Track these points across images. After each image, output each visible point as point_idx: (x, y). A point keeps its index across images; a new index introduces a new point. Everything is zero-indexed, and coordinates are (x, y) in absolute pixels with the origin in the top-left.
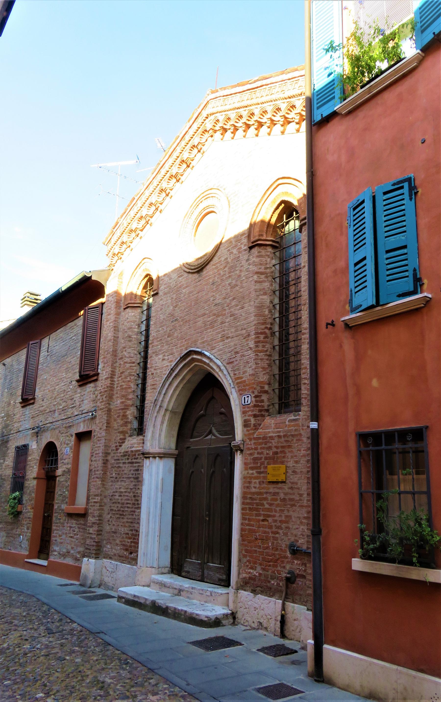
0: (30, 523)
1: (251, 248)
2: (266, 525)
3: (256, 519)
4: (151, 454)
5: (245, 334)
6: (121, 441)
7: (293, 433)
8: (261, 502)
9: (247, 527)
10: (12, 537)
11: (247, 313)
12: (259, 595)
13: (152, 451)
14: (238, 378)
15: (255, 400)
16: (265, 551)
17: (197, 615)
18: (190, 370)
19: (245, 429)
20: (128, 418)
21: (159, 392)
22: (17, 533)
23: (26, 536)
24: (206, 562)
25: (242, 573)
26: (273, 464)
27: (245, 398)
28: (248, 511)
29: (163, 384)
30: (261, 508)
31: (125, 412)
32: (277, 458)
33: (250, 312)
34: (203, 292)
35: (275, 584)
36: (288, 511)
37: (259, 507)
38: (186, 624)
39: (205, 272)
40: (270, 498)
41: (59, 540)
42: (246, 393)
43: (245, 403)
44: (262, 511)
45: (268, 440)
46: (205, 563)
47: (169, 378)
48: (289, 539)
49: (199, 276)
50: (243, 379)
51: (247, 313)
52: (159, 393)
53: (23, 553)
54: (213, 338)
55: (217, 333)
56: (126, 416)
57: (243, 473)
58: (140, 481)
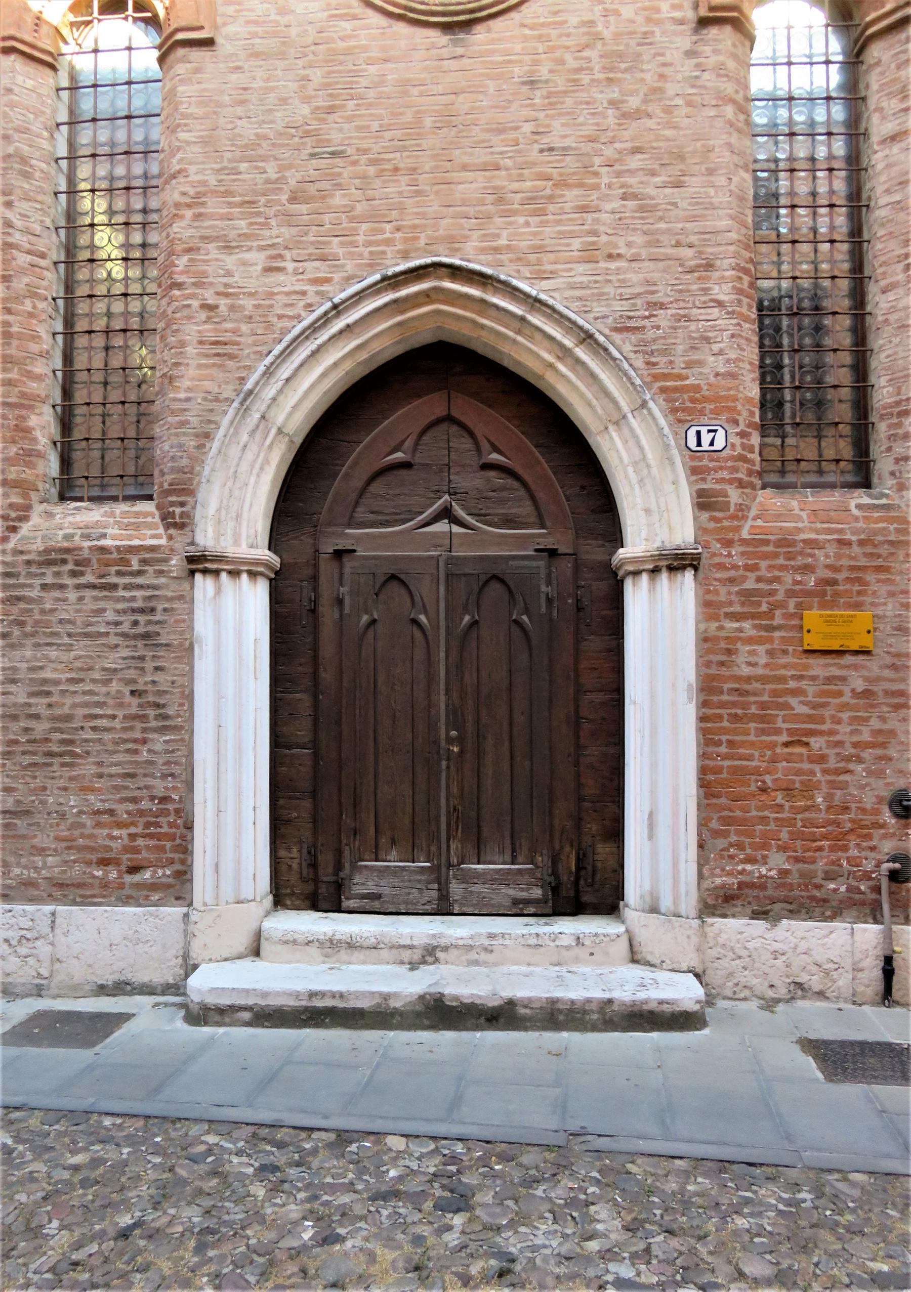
1: (704, 23)
2: (802, 755)
3: (762, 742)
4: (228, 563)
5: (691, 259)
6: (13, 515)
7: (892, 538)
8: (780, 700)
9: (727, 763)
11: (697, 203)
12: (785, 922)
13: (231, 550)
14: (665, 377)
16: (799, 816)
17: (661, 1002)
18: (399, 324)
19: (705, 516)
20: (35, 440)
21: (268, 368)
24: (455, 860)
25: (713, 875)
26: (819, 609)
27: (698, 433)
28: (726, 724)
29: (288, 346)
30: (777, 715)
31: (24, 418)
32: (836, 594)
33: (711, 203)
34: (481, 97)
35: (843, 889)
36: (883, 719)
37: (769, 712)
38: (616, 1034)
39: (480, 35)
40: (811, 690)
42: (705, 420)
43: (699, 444)
44: (784, 722)
45: (798, 549)
46: (449, 865)
47: (314, 331)
48: (888, 784)
49: (455, 43)
50: (687, 382)
51: (697, 203)
52: (265, 373)
54: (541, 246)
55: (560, 232)
56: (28, 431)
57: (703, 626)
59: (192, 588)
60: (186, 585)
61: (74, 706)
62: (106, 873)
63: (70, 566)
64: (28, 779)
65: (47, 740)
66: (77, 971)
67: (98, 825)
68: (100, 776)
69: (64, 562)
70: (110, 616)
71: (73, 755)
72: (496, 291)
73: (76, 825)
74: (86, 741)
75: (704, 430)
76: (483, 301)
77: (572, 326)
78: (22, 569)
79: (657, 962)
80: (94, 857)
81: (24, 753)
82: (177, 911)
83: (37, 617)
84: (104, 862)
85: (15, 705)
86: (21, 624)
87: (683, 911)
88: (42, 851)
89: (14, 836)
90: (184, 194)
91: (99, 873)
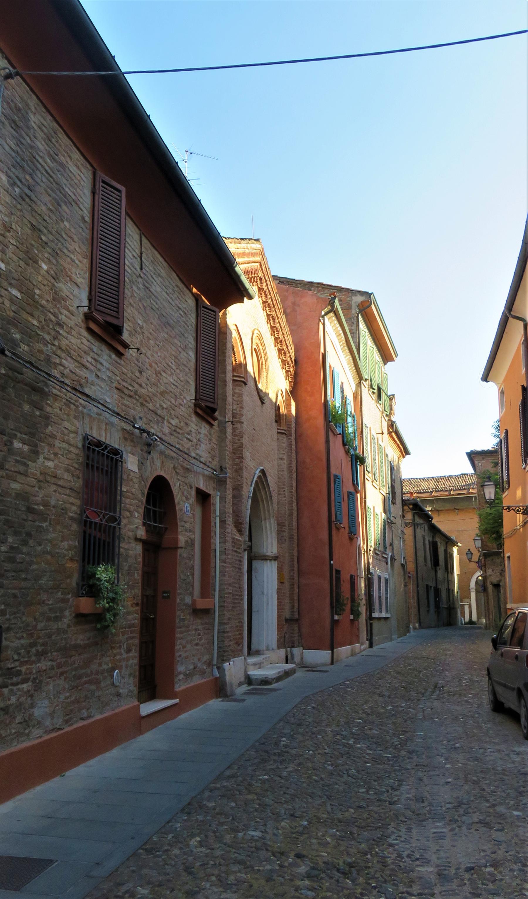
0: (133, 638)
10: (90, 682)
15: (37, 447)
22: (105, 667)
23: (127, 667)
41: (183, 655)
53: (123, 708)
58: (407, 630)
82: (243, 657)
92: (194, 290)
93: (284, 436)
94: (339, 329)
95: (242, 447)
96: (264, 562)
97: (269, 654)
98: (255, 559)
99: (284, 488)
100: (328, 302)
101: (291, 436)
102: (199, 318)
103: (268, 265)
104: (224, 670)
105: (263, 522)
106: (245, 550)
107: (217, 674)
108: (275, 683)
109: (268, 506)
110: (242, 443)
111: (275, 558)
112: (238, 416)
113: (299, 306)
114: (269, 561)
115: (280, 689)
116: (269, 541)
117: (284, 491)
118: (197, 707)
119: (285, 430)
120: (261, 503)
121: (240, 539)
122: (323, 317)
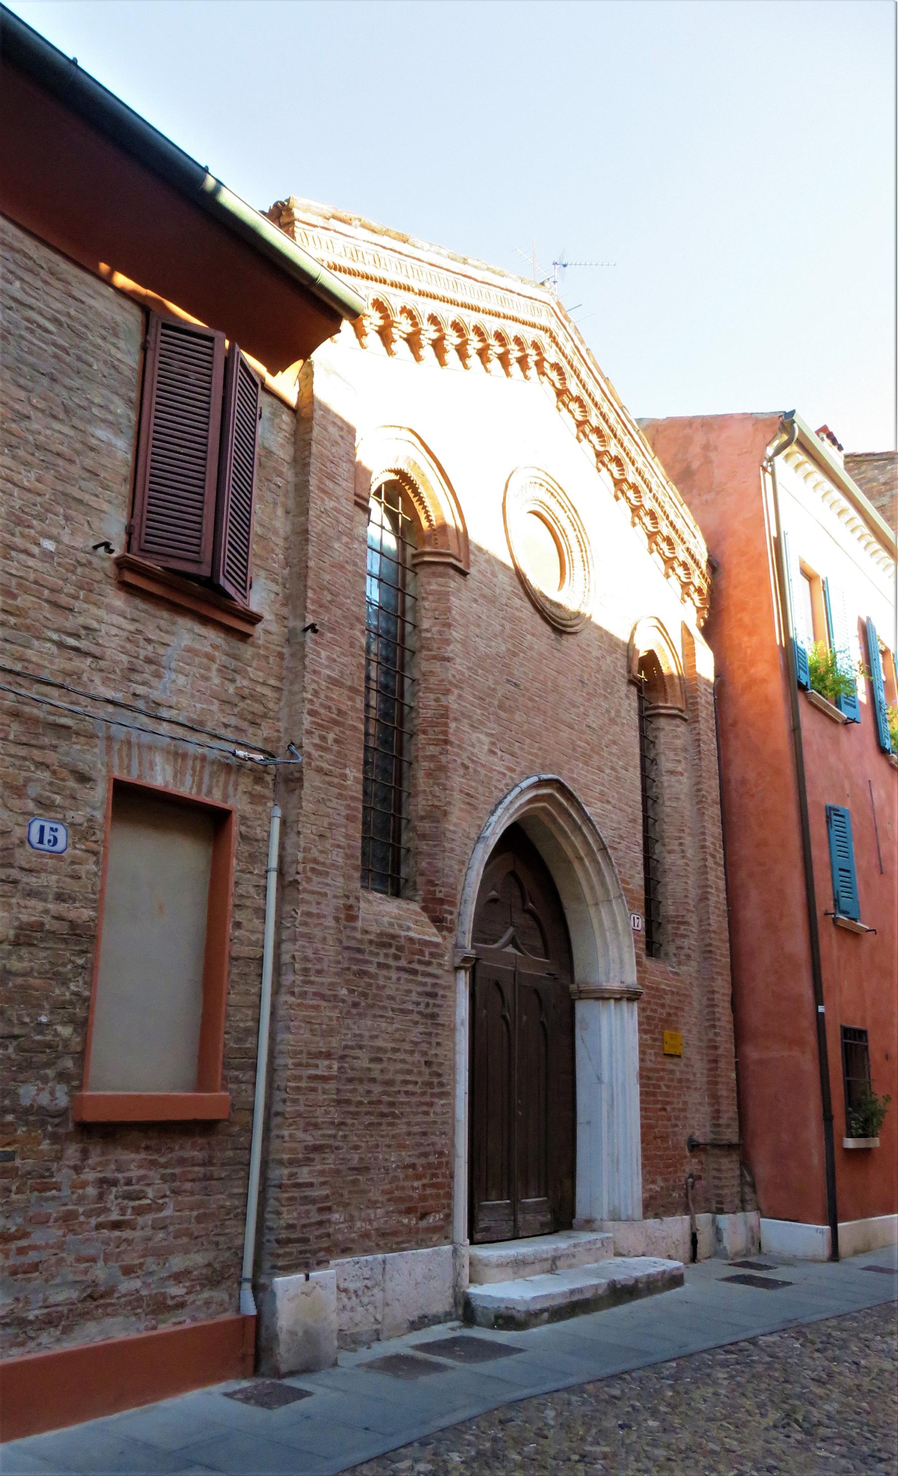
27: (42, 828)
59: (456, 980)
60: (452, 978)
61: (397, 1072)
62: (410, 1220)
63: (393, 951)
64: (368, 1138)
65: (380, 1102)
66: (401, 1314)
67: (406, 1178)
68: (409, 1134)
69: (390, 945)
70: (414, 997)
71: (393, 1114)
72: (572, 805)
73: (395, 1179)
74: (402, 1103)
75: (48, 826)
76: (567, 810)
77: (599, 840)
78: (366, 947)
79: (625, 1252)
80: (402, 1207)
81: (367, 1113)
82: (448, 1248)
83: (375, 991)
84: (409, 1211)
85: (362, 1068)
86: (365, 995)
87: (636, 1217)
88: (373, 1204)
89: (357, 1192)
90: (454, 676)
91: (406, 1221)
92: (121, 280)
93: (678, 721)
94: (837, 494)
95: (445, 716)
96: (600, 1003)
97: (612, 1231)
98: (580, 998)
99: (680, 838)
100: (778, 426)
101: (698, 722)
102: (150, 354)
103: (582, 342)
104: (273, 1295)
105: (592, 910)
106: (457, 969)
107: (250, 1308)
108: (548, 1322)
109: (599, 872)
110: (447, 708)
111: (632, 996)
112: (435, 646)
113: (716, 448)
114: (612, 1002)
115: (520, 1350)
116: (613, 952)
117: (681, 844)
118: (83, 1420)
119: (681, 711)
120: (576, 865)
121: (439, 940)
122: (771, 460)
